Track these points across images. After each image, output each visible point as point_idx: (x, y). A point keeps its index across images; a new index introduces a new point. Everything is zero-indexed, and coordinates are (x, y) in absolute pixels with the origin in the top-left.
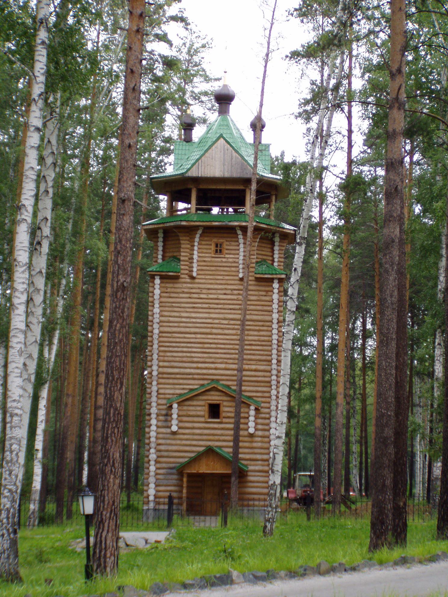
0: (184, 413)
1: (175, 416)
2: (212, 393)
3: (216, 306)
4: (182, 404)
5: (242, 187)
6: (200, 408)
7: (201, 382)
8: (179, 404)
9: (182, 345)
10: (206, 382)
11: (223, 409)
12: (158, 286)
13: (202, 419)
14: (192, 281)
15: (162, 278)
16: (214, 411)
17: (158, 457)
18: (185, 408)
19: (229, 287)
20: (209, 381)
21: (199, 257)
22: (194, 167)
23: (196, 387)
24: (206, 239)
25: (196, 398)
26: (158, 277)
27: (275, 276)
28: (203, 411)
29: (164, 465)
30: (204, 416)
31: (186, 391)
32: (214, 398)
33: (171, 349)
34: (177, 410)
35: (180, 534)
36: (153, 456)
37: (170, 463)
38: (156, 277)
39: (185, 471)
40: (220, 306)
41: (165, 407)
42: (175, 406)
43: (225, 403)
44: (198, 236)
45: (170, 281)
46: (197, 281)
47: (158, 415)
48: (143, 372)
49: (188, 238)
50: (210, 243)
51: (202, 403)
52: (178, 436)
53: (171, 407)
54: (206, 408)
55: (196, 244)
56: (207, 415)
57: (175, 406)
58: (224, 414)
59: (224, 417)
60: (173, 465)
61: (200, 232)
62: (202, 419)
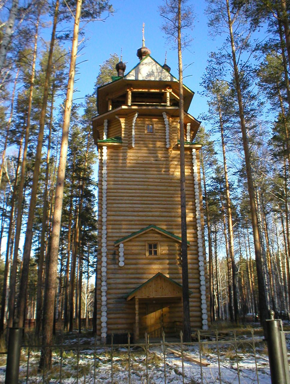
17: (108, 289)
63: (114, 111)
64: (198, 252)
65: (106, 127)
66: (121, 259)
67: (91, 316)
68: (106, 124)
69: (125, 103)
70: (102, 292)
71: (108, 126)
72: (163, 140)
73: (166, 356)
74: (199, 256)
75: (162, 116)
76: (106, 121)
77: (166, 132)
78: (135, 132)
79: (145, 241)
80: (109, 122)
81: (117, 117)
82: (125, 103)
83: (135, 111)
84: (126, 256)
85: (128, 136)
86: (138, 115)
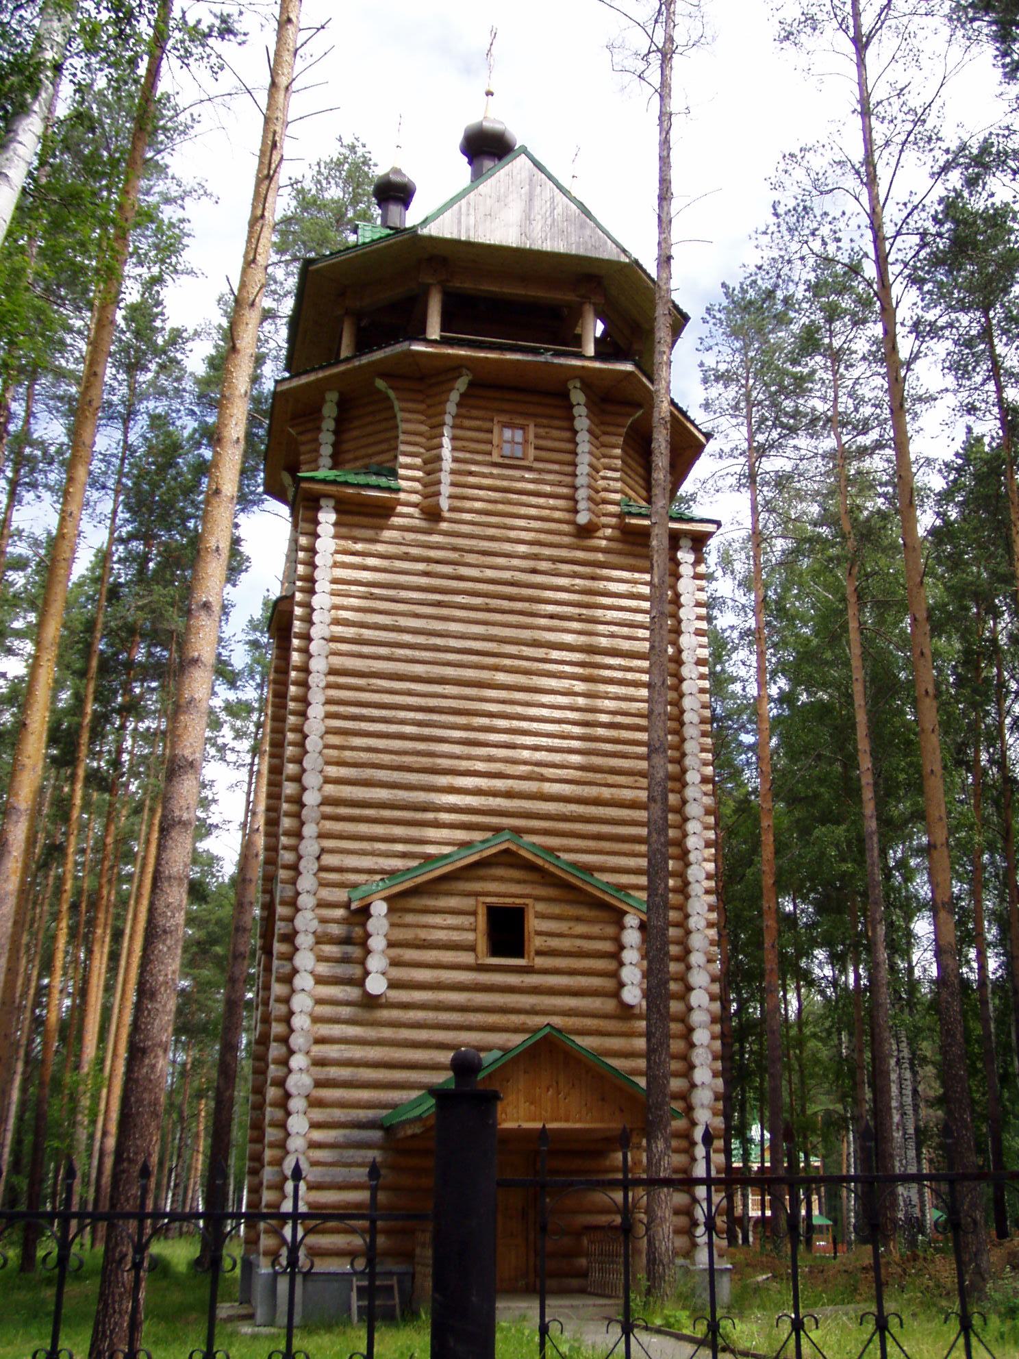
0: (407, 934)
1: (377, 943)
2: (500, 872)
3: (506, 604)
4: (402, 903)
5: (570, 297)
6: (457, 923)
7: (461, 835)
8: (396, 902)
9: (402, 714)
10: (477, 836)
11: (533, 923)
12: (332, 530)
13: (467, 958)
14: (432, 525)
15: (345, 508)
16: (506, 931)
17: (319, 1084)
18: (410, 918)
19: (547, 551)
20: (489, 835)
21: (455, 460)
22: (448, 214)
23: (446, 850)
24: (475, 413)
25: (445, 887)
26: (332, 503)
27: (33, 984)
28: (476, 932)
29: (338, 1114)
30: (472, 948)
31: (414, 863)
32: (503, 889)
33: (364, 726)
34: (385, 922)
35: (168, 99)
36: (300, 1081)
37: (357, 1105)
38: (323, 502)
39: (142, 407)
40: (519, 605)
41: (340, 913)
42: (379, 908)
43: (540, 907)
44: (454, 397)
45: (365, 520)
46: (444, 526)
47: (320, 939)
48: (770, 1124)
49: (422, 407)
50: (487, 425)
51: (468, 903)
52: (385, 1014)
53: (364, 913)
54: (482, 921)
55: (448, 419)
56: (482, 945)
57: (379, 908)
58: (538, 942)
59: (539, 953)
60: (370, 1114)
61: (461, 384)
62: (467, 958)
63: (365, 360)
64: (622, 948)
65: (329, 424)
66: (376, 963)
67: (958, 938)
68: (330, 410)
69: (419, 334)
70: (291, 1052)
71: (339, 421)
72: (568, 479)
73: (381, 1240)
74: (621, 964)
75: (565, 395)
76: (332, 397)
77: (579, 460)
78: (454, 449)
79: (477, 894)
80: (342, 405)
81: (380, 384)
82: (419, 334)
83: (454, 368)
84: (394, 952)
85: (425, 462)
86: (471, 384)
